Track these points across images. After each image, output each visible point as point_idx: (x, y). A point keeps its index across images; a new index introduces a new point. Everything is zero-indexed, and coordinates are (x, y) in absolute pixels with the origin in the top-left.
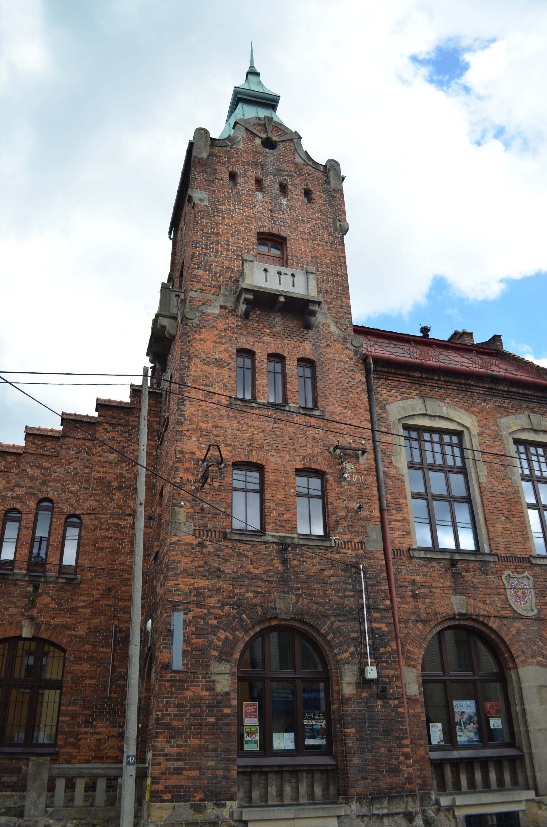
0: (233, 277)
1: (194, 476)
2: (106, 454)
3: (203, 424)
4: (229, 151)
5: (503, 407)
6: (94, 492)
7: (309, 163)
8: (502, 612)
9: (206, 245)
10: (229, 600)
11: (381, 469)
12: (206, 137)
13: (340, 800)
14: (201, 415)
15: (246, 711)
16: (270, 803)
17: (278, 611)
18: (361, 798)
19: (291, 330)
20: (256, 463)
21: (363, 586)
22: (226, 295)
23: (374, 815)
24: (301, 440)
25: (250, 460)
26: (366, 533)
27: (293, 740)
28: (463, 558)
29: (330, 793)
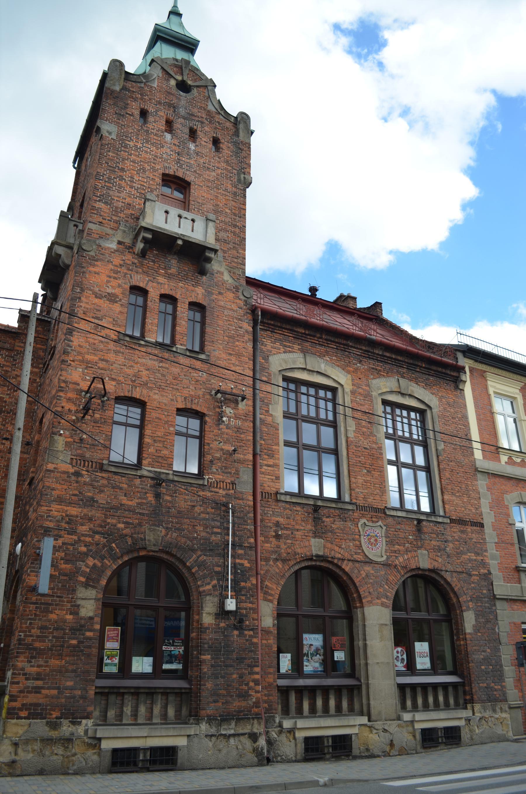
0: (134, 215)
1: (76, 406)
4: (143, 88)
5: (376, 369)
7: (221, 112)
8: (355, 556)
9: (109, 178)
10: (101, 529)
11: (258, 416)
12: (121, 69)
13: (191, 721)
14: (88, 347)
16: (124, 722)
17: (147, 543)
18: (211, 719)
19: (185, 273)
20: (139, 399)
21: (231, 524)
25: (133, 396)
26: (238, 474)
27: (152, 664)
28: (325, 505)
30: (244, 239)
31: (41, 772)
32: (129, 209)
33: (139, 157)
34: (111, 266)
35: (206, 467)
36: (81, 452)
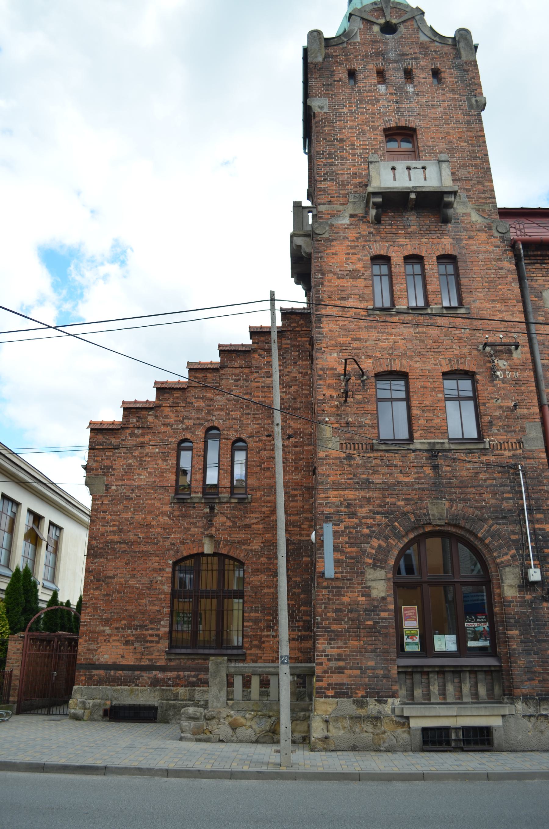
0: (362, 182)
1: (337, 391)
2: (264, 379)
3: (341, 339)
4: (346, 48)
6: (256, 416)
7: (435, 39)
9: (330, 154)
10: (380, 509)
11: (539, 362)
12: (320, 38)
13: (506, 700)
14: (338, 330)
15: (405, 614)
16: (433, 701)
17: (431, 518)
18: (527, 699)
19: (427, 227)
21: (523, 487)
22: (354, 203)
23: (542, 715)
24: (447, 342)
25: (393, 369)
27: (455, 642)
29: (495, 693)
30: (489, 169)
31: (354, 748)
32: (356, 179)
33: (355, 121)
34: (347, 242)
35: (485, 430)
36: (350, 435)
